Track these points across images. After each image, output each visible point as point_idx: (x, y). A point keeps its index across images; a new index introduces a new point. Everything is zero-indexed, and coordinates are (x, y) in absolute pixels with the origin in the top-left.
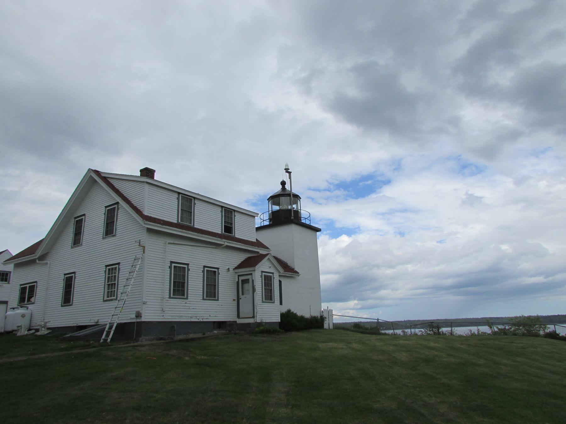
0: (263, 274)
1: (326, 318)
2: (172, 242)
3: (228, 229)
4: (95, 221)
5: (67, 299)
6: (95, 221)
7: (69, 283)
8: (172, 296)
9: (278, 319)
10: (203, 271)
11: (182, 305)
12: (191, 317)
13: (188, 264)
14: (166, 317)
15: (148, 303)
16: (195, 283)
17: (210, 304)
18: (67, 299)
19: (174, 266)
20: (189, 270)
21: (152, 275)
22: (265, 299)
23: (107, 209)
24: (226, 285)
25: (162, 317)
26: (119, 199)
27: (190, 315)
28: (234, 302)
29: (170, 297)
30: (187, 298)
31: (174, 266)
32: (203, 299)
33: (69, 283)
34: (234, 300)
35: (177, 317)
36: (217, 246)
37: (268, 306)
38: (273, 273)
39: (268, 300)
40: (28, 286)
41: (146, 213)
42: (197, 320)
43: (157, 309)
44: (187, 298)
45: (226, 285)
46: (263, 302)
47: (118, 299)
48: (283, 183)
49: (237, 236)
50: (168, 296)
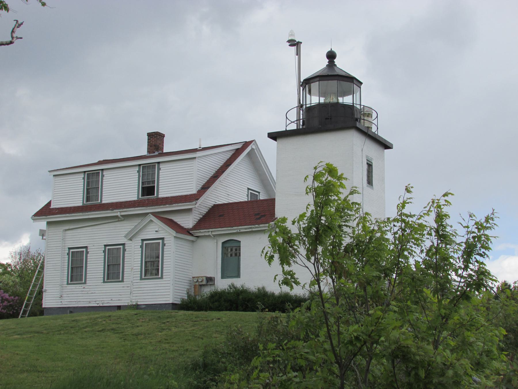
2: (67, 228)
3: (148, 190)
8: (69, 282)
11: (80, 290)
12: (90, 302)
13: (86, 247)
14: (64, 303)
15: (47, 291)
19: (83, 251)
21: (51, 265)
25: (61, 303)
27: (89, 300)
29: (68, 284)
30: (85, 283)
32: (104, 282)
35: (74, 303)
41: (194, 191)
42: (96, 305)
43: (56, 296)
44: (85, 283)
47: (340, 304)
48: (331, 56)
49: (106, 199)
50: (66, 283)
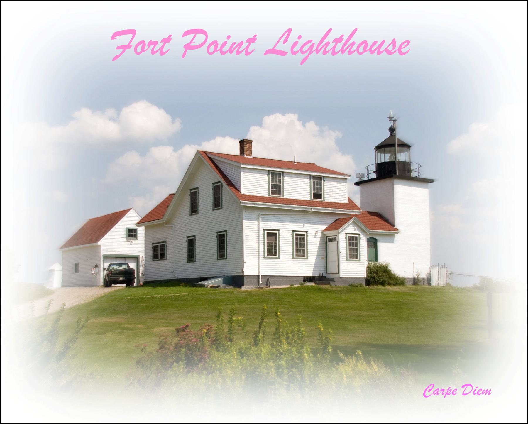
0: (348, 235)
1: (241, 288)
2: (264, 214)
4: (206, 199)
5: (191, 256)
6: (206, 199)
7: (191, 242)
9: (364, 274)
10: (293, 235)
16: (286, 244)
17: (300, 262)
18: (191, 256)
19: (267, 233)
20: (279, 235)
22: (350, 257)
23: (219, 234)
24: (313, 245)
26: (222, 180)
28: (323, 260)
31: (267, 233)
33: (191, 242)
34: (323, 258)
36: (305, 213)
37: (354, 264)
38: (359, 234)
39: (353, 257)
40: (159, 244)
45: (313, 245)
46: (347, 260)
